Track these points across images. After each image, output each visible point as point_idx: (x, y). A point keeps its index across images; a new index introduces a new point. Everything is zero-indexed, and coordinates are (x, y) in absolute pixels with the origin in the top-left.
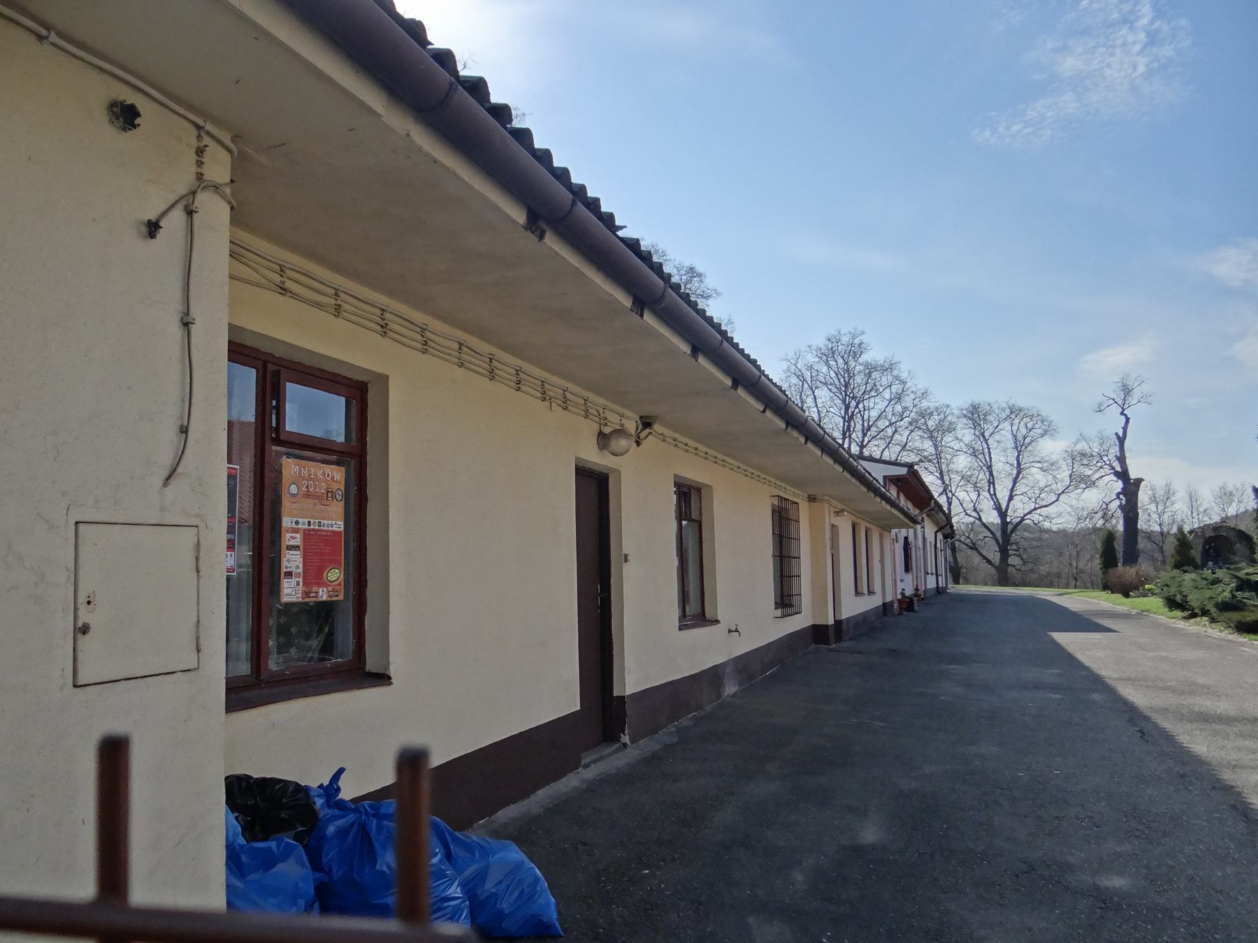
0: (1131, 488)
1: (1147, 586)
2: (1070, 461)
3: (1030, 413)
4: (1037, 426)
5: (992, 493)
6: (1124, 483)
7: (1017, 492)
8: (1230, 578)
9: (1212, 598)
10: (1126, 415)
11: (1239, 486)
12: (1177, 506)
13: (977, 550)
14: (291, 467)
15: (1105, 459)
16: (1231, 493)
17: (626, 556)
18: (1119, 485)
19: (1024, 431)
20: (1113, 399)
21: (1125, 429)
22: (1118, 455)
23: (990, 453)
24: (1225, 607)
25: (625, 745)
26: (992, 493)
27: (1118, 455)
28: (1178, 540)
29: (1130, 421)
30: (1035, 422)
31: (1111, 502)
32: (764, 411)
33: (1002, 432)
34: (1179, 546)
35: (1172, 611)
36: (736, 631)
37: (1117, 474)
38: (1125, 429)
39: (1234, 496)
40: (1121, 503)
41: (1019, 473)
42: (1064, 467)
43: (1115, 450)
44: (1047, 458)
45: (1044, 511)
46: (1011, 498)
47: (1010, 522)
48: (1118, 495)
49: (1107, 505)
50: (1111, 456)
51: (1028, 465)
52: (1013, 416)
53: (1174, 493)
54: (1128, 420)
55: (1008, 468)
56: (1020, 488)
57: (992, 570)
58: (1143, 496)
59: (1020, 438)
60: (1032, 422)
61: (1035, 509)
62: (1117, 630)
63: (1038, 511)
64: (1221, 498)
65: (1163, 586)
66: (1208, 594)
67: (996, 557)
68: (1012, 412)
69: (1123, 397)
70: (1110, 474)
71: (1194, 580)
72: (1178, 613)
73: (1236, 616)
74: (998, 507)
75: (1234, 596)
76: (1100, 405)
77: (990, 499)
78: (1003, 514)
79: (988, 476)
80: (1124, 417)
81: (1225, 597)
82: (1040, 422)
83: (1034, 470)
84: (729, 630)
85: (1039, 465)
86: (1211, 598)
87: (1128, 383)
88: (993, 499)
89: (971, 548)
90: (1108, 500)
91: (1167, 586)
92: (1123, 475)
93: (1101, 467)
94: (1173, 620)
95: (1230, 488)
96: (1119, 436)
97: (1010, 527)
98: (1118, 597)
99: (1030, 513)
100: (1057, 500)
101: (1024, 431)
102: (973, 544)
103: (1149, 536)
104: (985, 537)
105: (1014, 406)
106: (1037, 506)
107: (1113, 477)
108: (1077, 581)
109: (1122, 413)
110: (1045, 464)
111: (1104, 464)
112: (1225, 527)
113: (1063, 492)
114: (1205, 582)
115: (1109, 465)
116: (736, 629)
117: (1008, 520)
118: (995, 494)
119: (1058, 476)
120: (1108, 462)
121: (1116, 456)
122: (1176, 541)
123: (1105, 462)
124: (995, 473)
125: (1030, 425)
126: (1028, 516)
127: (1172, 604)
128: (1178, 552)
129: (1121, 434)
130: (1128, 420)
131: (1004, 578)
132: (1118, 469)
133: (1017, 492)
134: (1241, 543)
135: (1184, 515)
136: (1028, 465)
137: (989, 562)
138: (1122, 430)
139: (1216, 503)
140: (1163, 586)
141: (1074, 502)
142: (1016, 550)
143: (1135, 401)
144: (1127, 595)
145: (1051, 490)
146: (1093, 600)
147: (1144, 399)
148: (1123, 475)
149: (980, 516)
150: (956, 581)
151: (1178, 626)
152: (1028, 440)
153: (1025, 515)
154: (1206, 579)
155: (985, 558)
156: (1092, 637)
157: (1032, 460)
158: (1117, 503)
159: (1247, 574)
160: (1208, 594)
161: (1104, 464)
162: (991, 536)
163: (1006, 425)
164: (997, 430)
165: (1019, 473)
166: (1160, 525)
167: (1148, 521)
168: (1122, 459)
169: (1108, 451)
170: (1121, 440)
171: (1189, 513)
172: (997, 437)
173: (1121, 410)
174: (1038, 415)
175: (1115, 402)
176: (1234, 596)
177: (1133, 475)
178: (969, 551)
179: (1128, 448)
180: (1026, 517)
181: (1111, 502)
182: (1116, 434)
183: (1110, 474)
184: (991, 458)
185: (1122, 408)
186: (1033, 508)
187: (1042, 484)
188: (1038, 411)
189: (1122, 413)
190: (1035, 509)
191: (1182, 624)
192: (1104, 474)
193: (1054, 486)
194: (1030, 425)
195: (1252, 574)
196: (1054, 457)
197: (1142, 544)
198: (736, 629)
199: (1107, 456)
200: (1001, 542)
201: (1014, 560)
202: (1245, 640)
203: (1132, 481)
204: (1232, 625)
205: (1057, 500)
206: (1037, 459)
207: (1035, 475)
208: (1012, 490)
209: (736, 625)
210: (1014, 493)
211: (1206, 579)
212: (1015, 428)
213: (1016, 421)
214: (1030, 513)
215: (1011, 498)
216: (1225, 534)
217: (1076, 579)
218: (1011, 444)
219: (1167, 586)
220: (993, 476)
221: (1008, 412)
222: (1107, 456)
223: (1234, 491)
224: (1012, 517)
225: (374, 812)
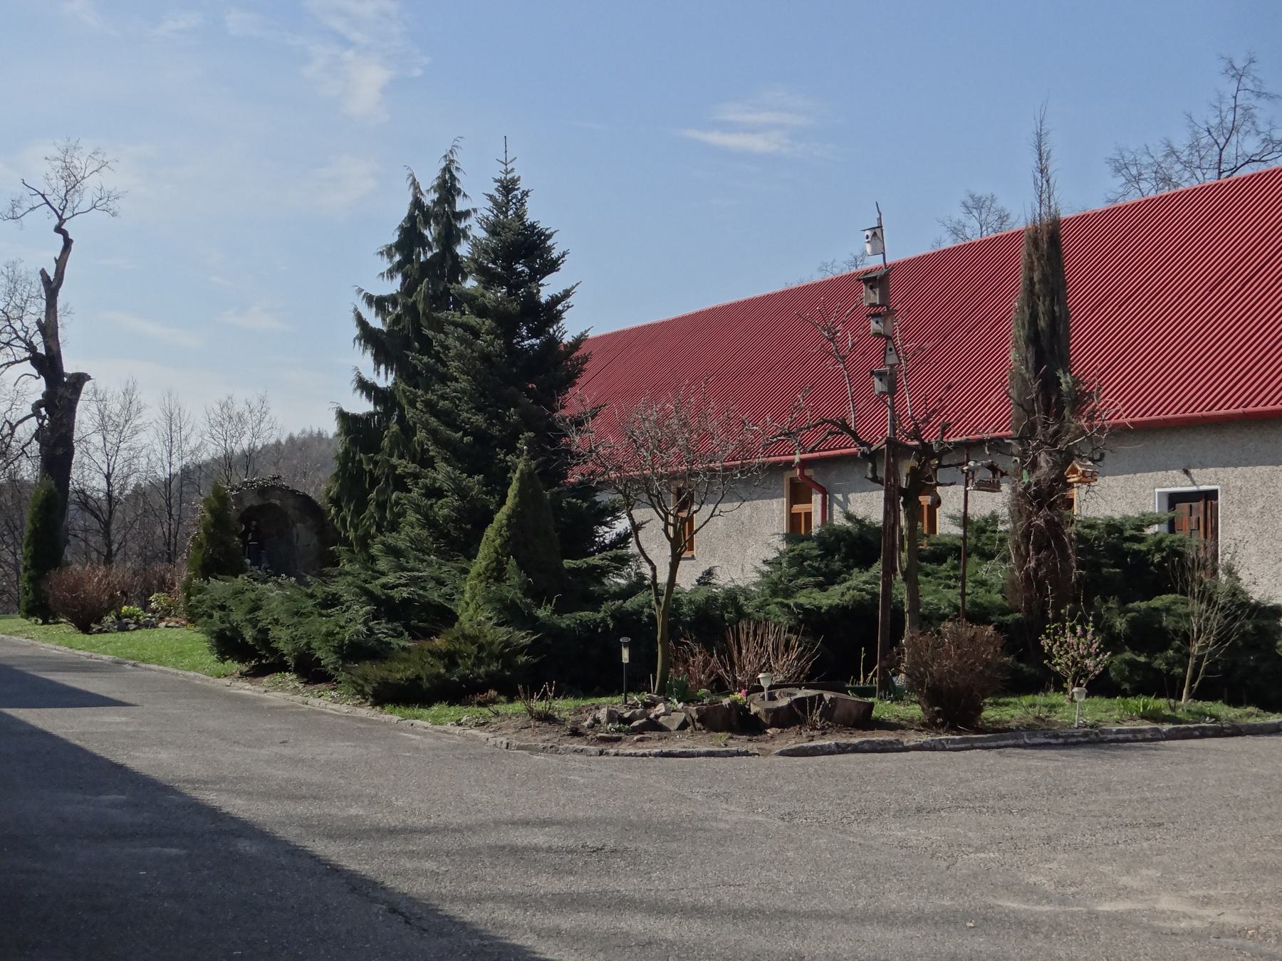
1: (125, 608)
6: (49, 383)
8: (355, 594)
10: (65, 233)
11: (255, 403)
12: (144, 438)
14: (1201, 504)
15: (17, 325)
16: (240, 416)
20: (43, 196)
21: (61, 263)
22: (43, 320)
24: (354, 652)
27: (43, 320)
28: (212, 511)
29: (73, 246)
31: (21, 421)
34: (213, 525)
35: (223, 661)
37: (36, 360)
38: (61, 263)
39: (246, 423)
40: (41, 425)
43: (37, 310)
49: (13, 428)
53: (139, 411)
58: (85, 417)
64: (222, 426)
66: (324, 625)
69: (62, 193)
70: (25, 359)
71: (289, 598)
72: (234, 666)
73: (373, 670)
76: (15, 204)
80: (61, 237)
81: (358, 633)
86: (330, 634)
87: (76, 163)
90: (14, 417)
92: (48, 364)
93: (8, 344)
94: (227, 681)
95: (239, 407)
96: (48, 277)
98: (65, 628)
103: (85, 501)
107: (28, 367)
109: (59, 229)
111: (14, 336)
114: (311, 602)
115: (24, 341)
120: (22, 334)
121: (39, 322)
122: (208, 515)
123: (15, 332)
128: (210, 537)
129: (52, 275)
132: (41, 350)
138: (55, 265)
139: (213, 437)
143: (85, 205)
144: (85, 629)
146: (15, 638)
147: (104, 202)
148: (48, 364)
151: (242, 692)
154: (312, 596)
156: (107, 719)
158: (33, 424)
159: (384, 586)
161: (14, 336)
166: (108, 477)
168: (49, 329)
169: (23, 309)
170: (52, 287)
171: (166, 454)
173: (56, 221)
175: (48, 203)
179: (66, 307)
181: (21, 421)
182: (43, 273)
183: (25, 359)
185: (60, 217)
189: (59, 229)
191: (246, 688)
192: (12, 359)
195: (397, 586)
197: (75, 518)
199: (20, 318)
202: (395, 718)
203: (65, 379)
204: (368, 689)
216: (278, 502)
219: (223, 608)
222: (20, 318)
223: (247, 414)
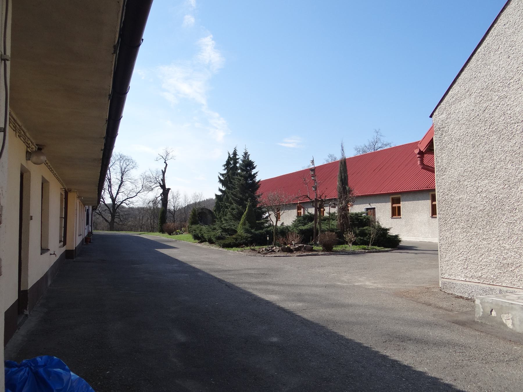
0: (166, 192)
2: (142, 180)
3: (128, 158)
4: (130, 164)
5: (110, 191)
7: (120, 191)
9: (215, 235)
10: (166, 163)
12: (180, 200)
13: (102, 215)
15: (158, 180)
17: (31, 217)
18: (161, 191)
19: (125, 165)
21: (165, 168)
23: (110, 174)
24: (219, 238)
25: (27, 315)
26: (110, 191)
30: (130, 162)
32: (102, 150)
33: (116, 165)
36: (54, 254)
37: (161, 186)
38: (165, 168)
41: (122, 183)
42: (140, 182)
43: (161, 177)
44: (133, 178)
45: (130, 200)
46: (117, 194)
47: (117, 204)
48: (161, 194)
49: (157, 198)
50: (160, 179)
51: (125, 180)
52: (121, 159)
53: (180, 195)
54: (167, 165)
55: (117, 181)
56: (122, 189)
57: (107, 224)
58: (170, 196)
59: (123, 169)
60: (128, 162)
61: (127, 199)
62: (178, 247)
63: (128, 200)
65: (193, 230)
66: (213, 233)
67: (109, 219)
68: (121, 157)
71: (207, 229)
73: (223, 242)
74: (112, 197)
75: (222, 234)
77: (109, 193)
78: (114, 200)
79: (108, 183)
81: (219, 235)
82: (131, 163)
83: (127, 182)
84: (50, 254)
85: (130, 180)
86: (214, 235)
88: (110, 193)
89: (99, 214)
91: (195, 230)
92: (163, 186)
94: (195, 243)
95: (197, 194)
97: (116, 206)
99: (125, 200)
100: (136, 195)
101: (125, 165)
102: (100, 212)
103: (170, 211)
104: (105, 210)
105: (122, 154)
106: (128, 197)
107: (159, 187)
108: (142, 228)
109: (165, 162)
110: (133, 180)
112: (205, 208)
113: (139, 192)
116: (54, 253)
117: (116, 203)
118: (111, 192)
119: (137, 186)
120: (158, 181)
124: (112, 183)
125: (127, 163)
126: (124, 202)
127: (196, 237)
130: (167, 165)
131: (112, 228)
132: (162, 184)
133: (120, 191)
134: (209, 215)
135: (182, 203)
136: (125, 180)
137: (106, 221)
140: (193, 230)
141: (143, 197)
142: (118, 216)
143: (170, 158)
144: (170, 234)
145: (134, 191)
146: (157, 236)
148: (163, 186)
149: (104, 201)
150: (96, 229)
152: (126, 170)
153: (123, 201)
154: (211, 228)
155: (105, 219)
157: (127, 178)
158: (160, 198)
159: (224, 226)
160: (213, 233)
162: (108, 209)
163: (118, 163)
164: (114, 164)
165: (122, 183)
166: (174, 207)
167: (170, 206)
168: (163, 180)
170: (164, 173)
171: (184, 203)
172: (114, 167)
173: (164, 161)
174: (131, 160)
176: (222, 234)
177: (167, 187)
178: (98, 216)
180: (123, 202)
182: (162, 170)
184: (110, 176)
185: (165, 160)
186: (126, 198)
187: (131, 188)
188: (131, 158)
190: (127, 199)
191: (199, 245)
193: (135, 190)
194: (127, 163)
196: (136, 178)
197: (168, 214)
198: (54, 253)
200: (112, 212)
201: (116, 220)
202: (226, 250)
204: (221, 245)
205: (136, 195)
206: (129, 178)
207: (128, 185)
208: (118, 190)
209: (54, 251)
210: (119, 192)
211: (211, 228)
212: (121, 164)
213: (122, 161)
214: (125, 200)
215: (117, 194)
217: (141, 228)
218: (119, 170)
219: (195, 230)
220: (111, 183)
221: (119, 157)
222: (158, 178)
224: (117, 202)
225: (34, 365)
